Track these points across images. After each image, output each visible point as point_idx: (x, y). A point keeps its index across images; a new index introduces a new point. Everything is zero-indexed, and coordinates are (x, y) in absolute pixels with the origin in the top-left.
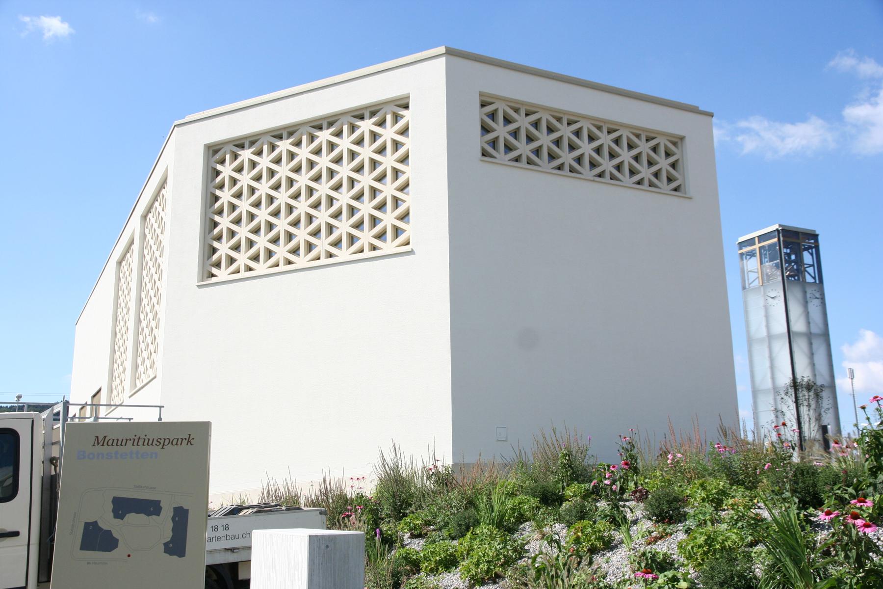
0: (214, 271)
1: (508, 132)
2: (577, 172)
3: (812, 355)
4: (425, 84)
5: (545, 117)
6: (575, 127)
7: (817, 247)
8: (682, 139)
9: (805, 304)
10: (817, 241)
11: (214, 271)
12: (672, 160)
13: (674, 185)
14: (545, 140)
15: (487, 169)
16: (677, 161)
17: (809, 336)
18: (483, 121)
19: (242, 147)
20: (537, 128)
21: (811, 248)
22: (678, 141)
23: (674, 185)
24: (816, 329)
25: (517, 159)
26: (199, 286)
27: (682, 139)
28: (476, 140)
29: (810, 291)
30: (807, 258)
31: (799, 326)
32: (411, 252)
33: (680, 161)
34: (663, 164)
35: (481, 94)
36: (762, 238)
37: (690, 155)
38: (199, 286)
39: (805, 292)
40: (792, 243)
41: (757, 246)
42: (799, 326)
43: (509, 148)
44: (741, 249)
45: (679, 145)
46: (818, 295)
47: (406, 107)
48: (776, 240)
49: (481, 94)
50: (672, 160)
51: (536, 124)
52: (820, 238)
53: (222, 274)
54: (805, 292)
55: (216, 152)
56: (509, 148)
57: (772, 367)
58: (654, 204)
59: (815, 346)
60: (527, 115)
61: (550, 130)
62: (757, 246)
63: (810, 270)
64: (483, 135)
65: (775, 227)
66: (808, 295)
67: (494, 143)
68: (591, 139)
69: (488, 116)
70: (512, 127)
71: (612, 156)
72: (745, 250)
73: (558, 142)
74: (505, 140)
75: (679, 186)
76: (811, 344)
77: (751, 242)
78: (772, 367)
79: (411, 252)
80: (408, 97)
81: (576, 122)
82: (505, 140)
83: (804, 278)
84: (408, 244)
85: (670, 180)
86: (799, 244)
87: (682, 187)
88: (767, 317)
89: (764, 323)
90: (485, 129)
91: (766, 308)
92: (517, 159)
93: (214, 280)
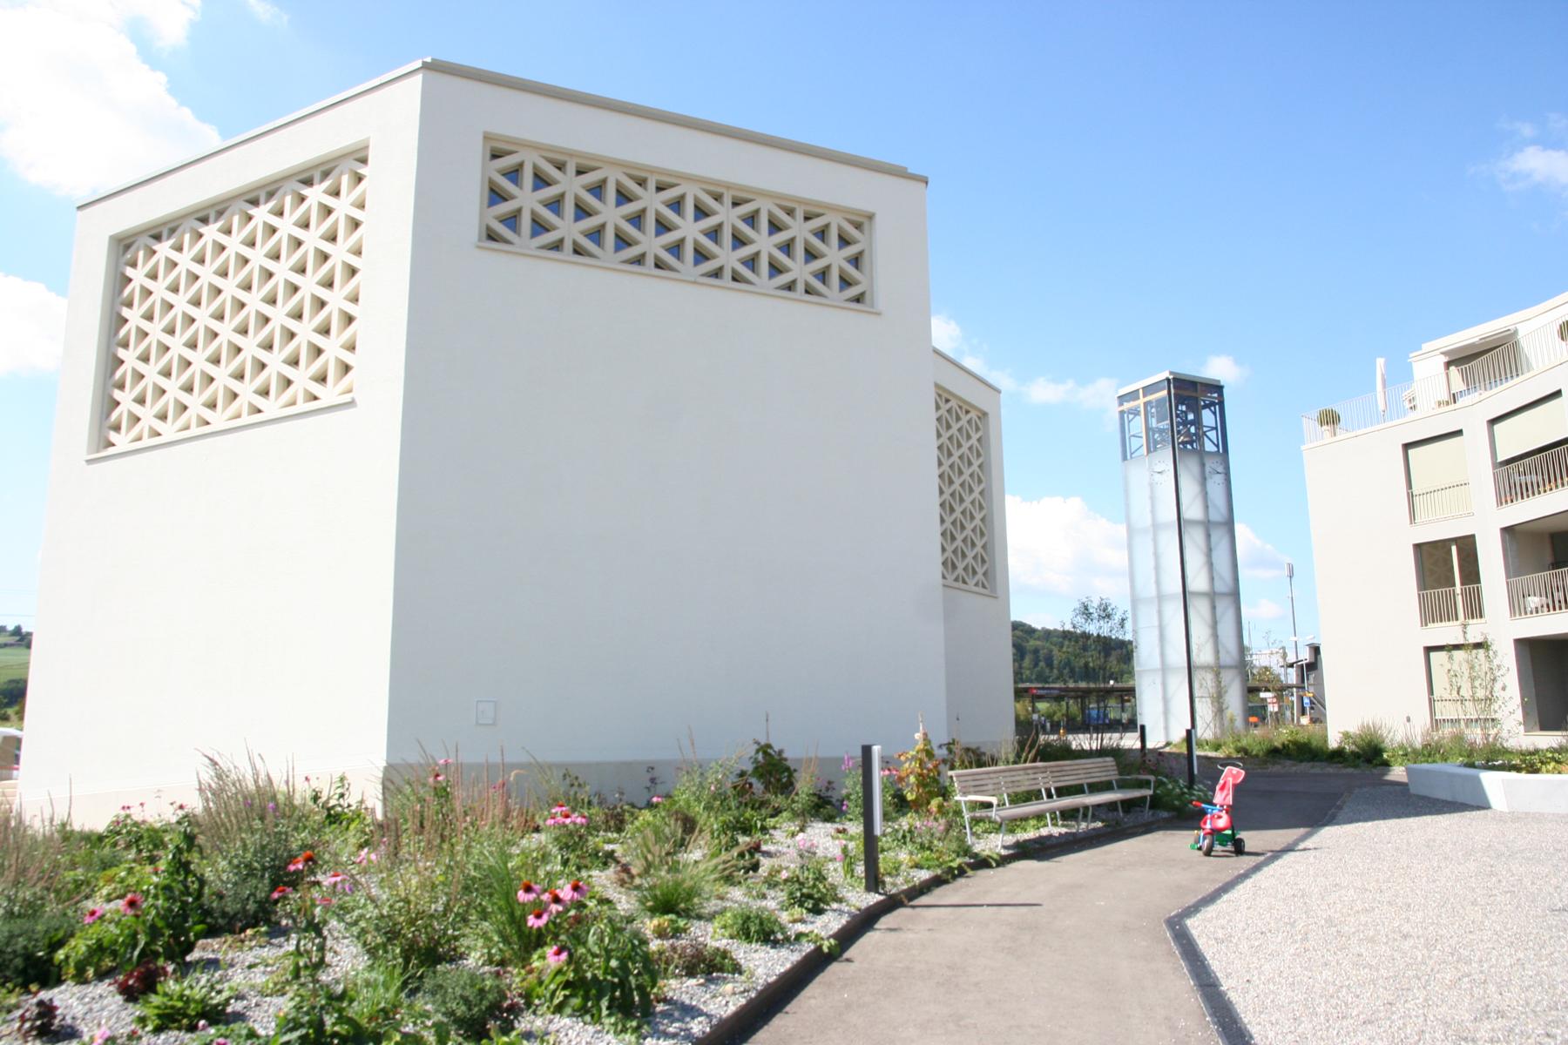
0: (113, 436)
1: (539, 198)
2: (818, 294)
3: (1209, 552)
4: (389, 122)
5: (613, 177)
6: (816, 223)
7: (1221, 404)
8: (871, 217)
9: (1203, 481)
10: (1221, 395)
11: (113, 436)
12: (851, 251)
13: (853, 291)
14: (764, 243)
15: (496, 262)
16: (861, 253)
17: (1207, 525)
18: (491, 182)
19: (158, 238)
20: (823, 240)
21: (1213, 404)
22: (862, 221)
23: (853, 291)
24: (1217, 514)
25: (790, 287)
26: (89, 462)
27: (871, 217)
28: (470, 210)
29: (1210, 464)
30: (1208, 417)
31: (1193, 511)
32: (352, 403)
33: (866, 254)
34: (835, 257)
35: (487, 137)
36: (1148, 390)
37: (883, 245)
38: (89, 462)
39: (1203, 465)
40: (1189, 398)
41: (1142, 400)
42: (1193, 511)
43: (701, 256)
44: (1121, 404)
45: (866, 227)
46: (1220, 469)
47: (364, 161)
48: (1165, 392)
49: (487, 137)
50: (851, 251)
51: (822, 234)
52: (1225, 391)
53: (121, 441)
54: (1203, 465)
55: (128, 247)
56: (701, 256)
57: (1157, 568)
58: (826, 320)
59: (1214, 539)
60: (807, 219)
61: (701, 212)
62: (1142, 400)
63: (1212, 434)
64: (492, 203)
65: (1166, 374)
66: (1208, 469)
67: (512, 220)
68: (775, 227)
69: (816, 234)
70: (782, 237)
71: (811, 255)
72: (1127, 406)
73: (787, 248)
74: (841, 270)
75: (863, 294)
76: (1208, 536)
77: (1133, 395)
78: (1157, 568)
79: (352, 403)
80: (366, 148)
81: (747, 201)
82: (841, 270)
83: (1202, 445)
84: (350, 391)
85: (846, 282)
86: (1196, 399)
87: (867, 296)
88: (1152, 498)
89: (1148, 508)
90: (496, 195)
91: (1152, 486)
92: (790, 287)
93: (111, 451)
